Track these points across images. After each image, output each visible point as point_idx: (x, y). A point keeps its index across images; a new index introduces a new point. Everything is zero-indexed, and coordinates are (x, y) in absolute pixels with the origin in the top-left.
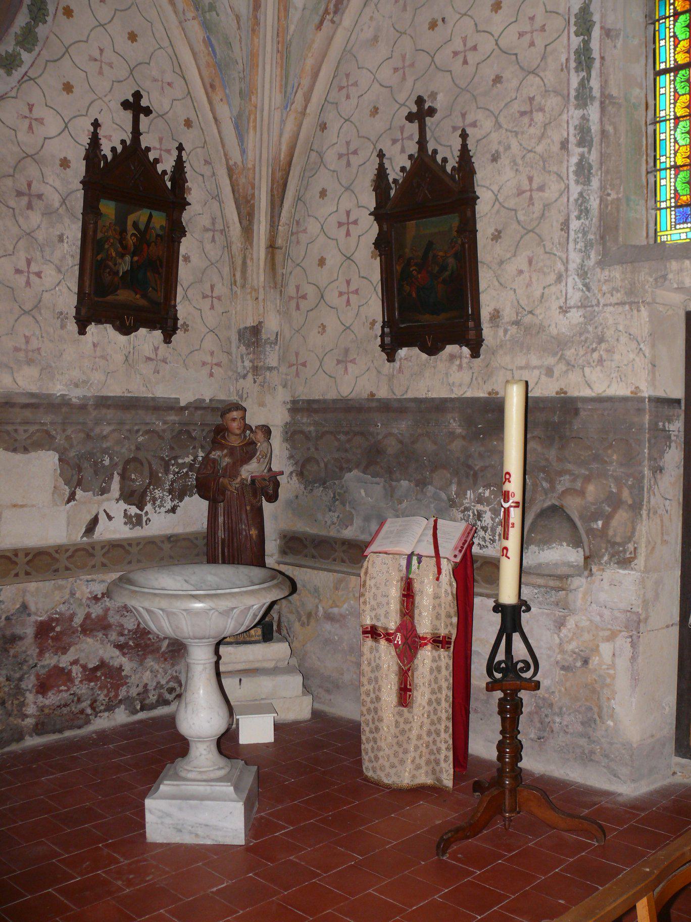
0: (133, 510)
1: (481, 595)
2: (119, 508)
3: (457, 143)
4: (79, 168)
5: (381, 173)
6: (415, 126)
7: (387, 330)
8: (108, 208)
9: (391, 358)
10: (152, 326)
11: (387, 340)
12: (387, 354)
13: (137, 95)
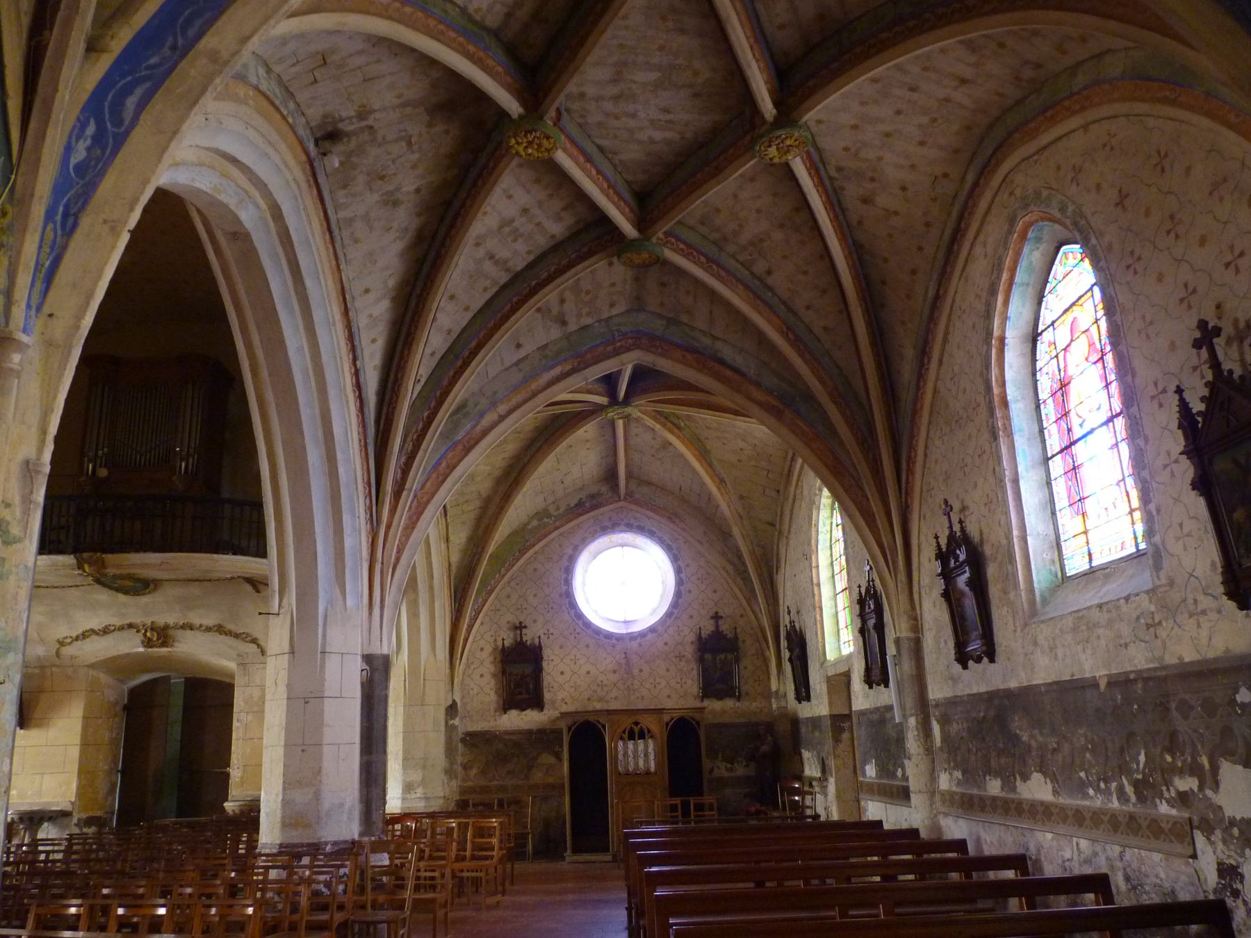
0: (729, 766)
8: (708, 656)
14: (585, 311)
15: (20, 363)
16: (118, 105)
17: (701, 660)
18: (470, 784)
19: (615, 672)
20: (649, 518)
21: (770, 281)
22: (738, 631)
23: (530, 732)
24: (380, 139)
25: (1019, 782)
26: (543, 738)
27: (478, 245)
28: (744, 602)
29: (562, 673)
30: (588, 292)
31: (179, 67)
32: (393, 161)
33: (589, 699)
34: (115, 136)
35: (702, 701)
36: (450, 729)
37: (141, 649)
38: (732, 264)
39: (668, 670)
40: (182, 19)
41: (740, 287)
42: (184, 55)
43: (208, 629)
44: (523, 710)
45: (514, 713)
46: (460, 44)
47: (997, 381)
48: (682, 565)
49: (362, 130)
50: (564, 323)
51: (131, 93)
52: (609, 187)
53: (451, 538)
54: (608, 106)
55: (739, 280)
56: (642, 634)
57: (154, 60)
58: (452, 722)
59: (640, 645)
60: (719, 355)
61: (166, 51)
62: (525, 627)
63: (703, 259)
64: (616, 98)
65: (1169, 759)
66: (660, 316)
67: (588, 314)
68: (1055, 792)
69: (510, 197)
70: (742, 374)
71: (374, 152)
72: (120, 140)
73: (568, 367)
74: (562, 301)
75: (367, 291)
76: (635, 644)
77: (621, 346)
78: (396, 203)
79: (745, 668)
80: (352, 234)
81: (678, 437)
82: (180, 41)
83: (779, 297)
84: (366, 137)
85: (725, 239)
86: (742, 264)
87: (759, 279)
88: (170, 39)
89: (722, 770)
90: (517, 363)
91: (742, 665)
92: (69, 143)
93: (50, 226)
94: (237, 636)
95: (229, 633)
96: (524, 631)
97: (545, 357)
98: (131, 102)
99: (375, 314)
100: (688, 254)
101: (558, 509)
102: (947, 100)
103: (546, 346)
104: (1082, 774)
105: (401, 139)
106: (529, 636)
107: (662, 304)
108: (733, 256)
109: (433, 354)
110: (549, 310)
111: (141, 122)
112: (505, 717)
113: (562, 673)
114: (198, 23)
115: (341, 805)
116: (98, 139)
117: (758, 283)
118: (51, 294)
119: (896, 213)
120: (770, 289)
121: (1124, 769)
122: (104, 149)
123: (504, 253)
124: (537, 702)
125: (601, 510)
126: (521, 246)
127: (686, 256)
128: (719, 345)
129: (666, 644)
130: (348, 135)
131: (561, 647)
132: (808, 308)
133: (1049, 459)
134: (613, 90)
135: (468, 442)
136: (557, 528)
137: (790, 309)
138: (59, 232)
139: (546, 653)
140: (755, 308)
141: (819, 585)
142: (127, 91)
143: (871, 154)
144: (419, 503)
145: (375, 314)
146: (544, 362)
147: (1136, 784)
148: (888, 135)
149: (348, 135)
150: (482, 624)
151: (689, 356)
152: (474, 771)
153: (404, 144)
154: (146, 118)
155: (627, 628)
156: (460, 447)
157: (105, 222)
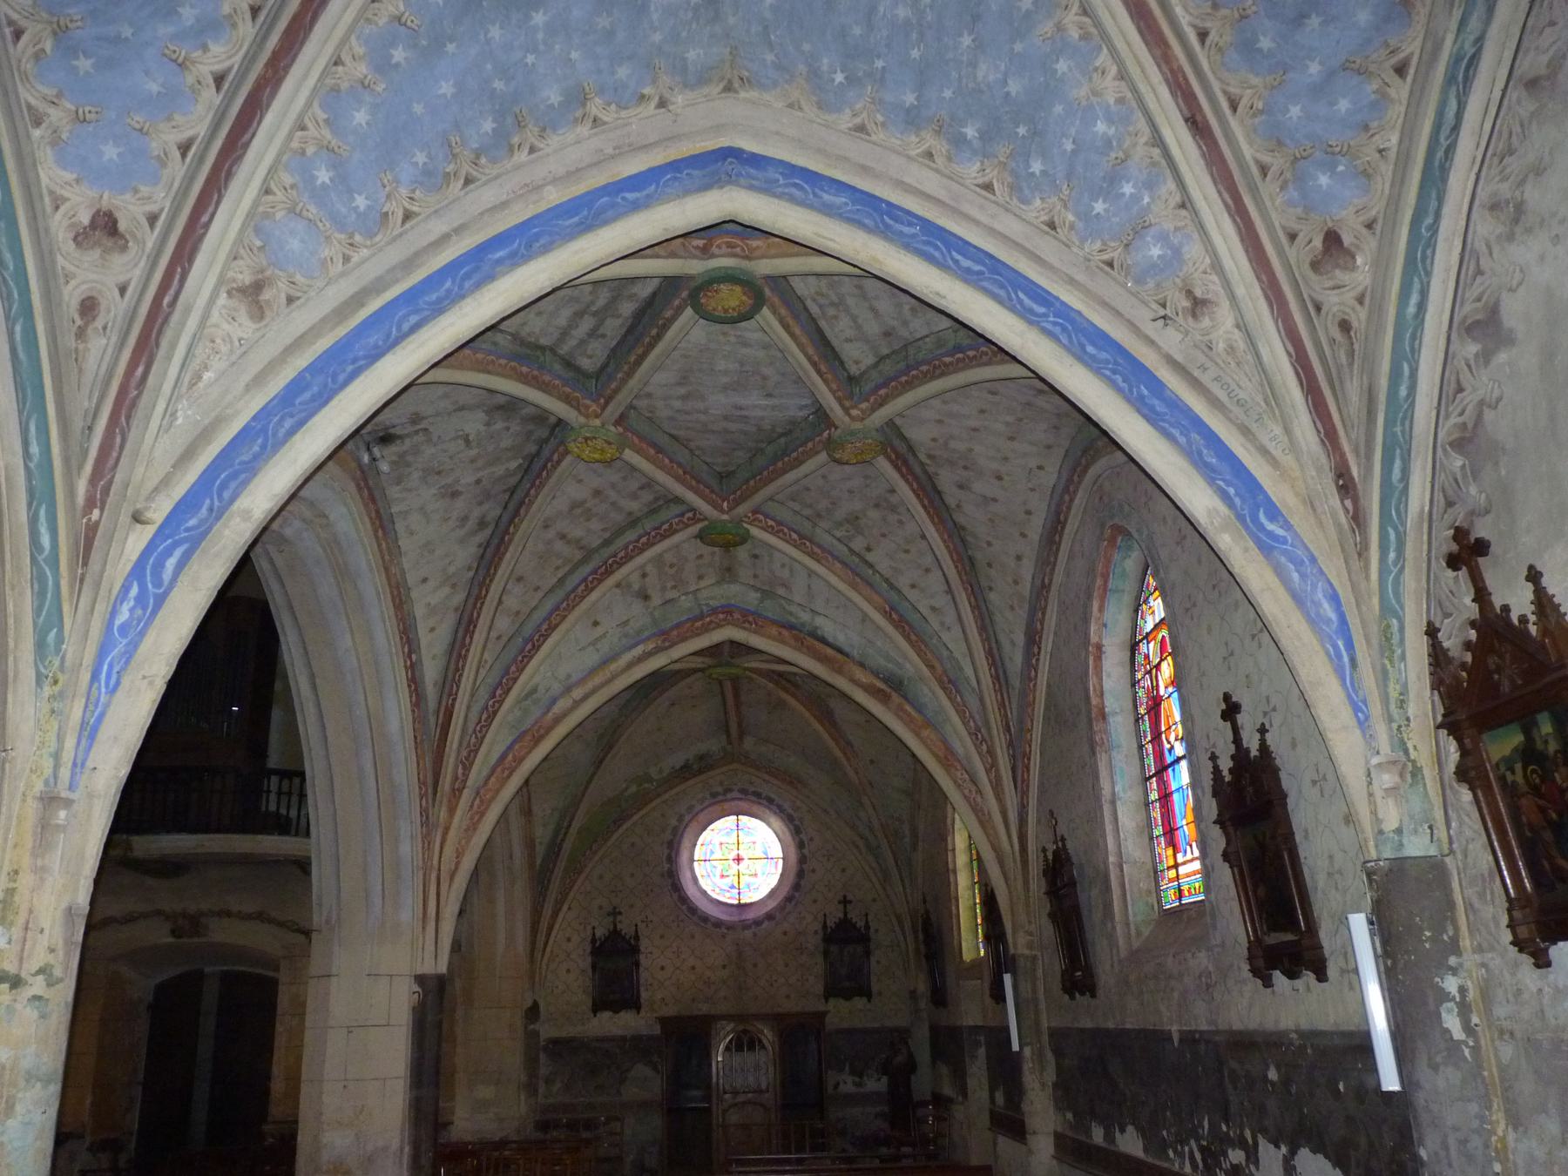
0: (857, 1079)
1: (267, 806)
2: (849, 1079)
3: (1528, 592)
4: (821, 933)
5: (1217, 771)
6: (1463, 573)
7: (1517, 914)
8: (834, 949)
9: (1542, 961)
10: (861, 995)
11: (1523, 932)
12: (1533, 955)
13: (845, 897)
14: (669, 585)
15: (66, 819)
16: (159, 566)
17: (826, 954)
18: (551, 1101)
19: (724, 967)
20: (767, 782)
21: (870, 557)
22: (870, 918)
23: (623, 1039)
24: (435, 439)
25: (1118, 1134)
26: (637, 1047)
27: (546, 527)
28: (878, 886)
29: (662, 968)
30: (671, 566)
31: (215, 528)
32: (451, 458)
33: (693, 1000)
34: (156, 596)
35: (827, 1001)
36: (532, 1036)
37: (171, 940)
38: (827, 540)
39: (787, 965)
40: (218, 482)
41: (838, 565)
42: (218, 518)
43: (249, 917)
44: (616, 1012)
45: (606, 1015)
46: (513, 369)
47: (1095, 690)
48: (805, 838)
49: (417, 432)
50: (646, 598)
51: (170, 555)
52: (685, 473)
53: (535, 808)
54: (677, 404)
55: (836, 558)
56: (757, 923)
57: (192, 522)
58: (532, 1027)
59: (755, 935)
60: (819, 633)
61: (204, 511)
62: (620, 913)
63: (795, 536)
64: (685, 398)
65: (1224, 1128)
66: (757, 589)
67: (674, 587)
68: (1146, 1150)
69: (580, 481)
70: (847, 655)
71: (429, 451)
72: (160, 600)
73: (651, 646)
74: (644, 575)
75: (425, 580)
76: (748, 934)
77: (711, 622)
78: (455, 494)
79: (878, 962)
80: (407, 527)
81: (793, 695)
82: (216, 503)
83: (881, 575)
84: (420, 438)
85: (819, 516)
86: (839, 540)
87: (858, 555)
88: (208, 502)
89: (848, 1084)
90: (593, 643)
91: (873, 960)
92: (114, 607)
93: (96, 685)
94: (281, 924)
95: (271, 921)
96: (619, 918)
97: (626, 636)
98: (171, 563)
99: (433, 603)
100: (778, 532)
101: (661, 771)
102: (1029, 404)
103: (625, 623)
104: (1165, 1133)
105: (458, 437)
106: (626, 928)
107: (755, 576)
108: (828, 532)
109: (499, 638)
110: (629, 586)
111: (179, 583)
112: (595, 1022)
113: (662, 968)
114: (233, 485)
115: (385, 1149)
116: (141, 600)
117: (857, 560)
118: (94, 750)
119: (994, 500)
120: (871, 566)
121: (1194, 1133)
122: (144, 609)
123: (577, 532)
124: (634, 1004)
125: (711, 773)
126: (595, 525)
127: (775, 533)
128: (819, 621)
129: (785, 933)
130: (400, 437)
131: (662, 937)
132: (927, 570)
133: (1166, 768)
134: (682, 391)
135: (538, 731)
136: (659, 795)
137: (892, 586)
138: (103, 690)
139: (644, 944)
140: (854, 586)
141: (955, 872)
142: (168, 552)
143: (961, 446)
144: (482, 801)
145: (433, 603)
146: (624, 641)
147: (1202, 1149)
148: (975, 430)
149: (400, 437)
150: (569, 909)
151: (785, 633)
152: (558, 1085)
153: (460, 442)
154: (184, 579)
155: (740, 914)
156: (528, 738)
157: (144, 677)
